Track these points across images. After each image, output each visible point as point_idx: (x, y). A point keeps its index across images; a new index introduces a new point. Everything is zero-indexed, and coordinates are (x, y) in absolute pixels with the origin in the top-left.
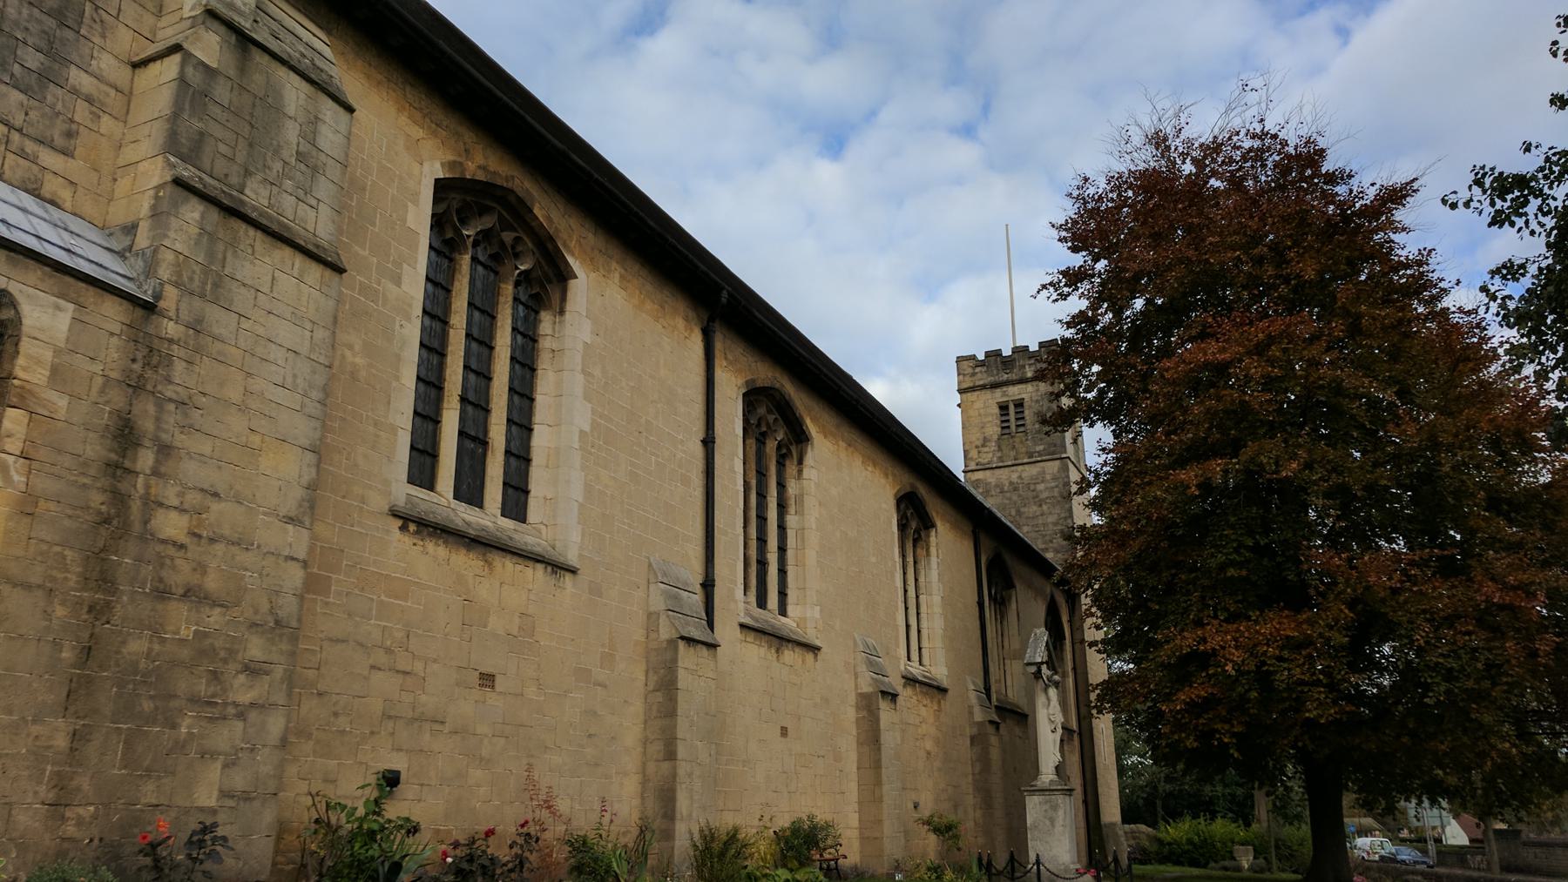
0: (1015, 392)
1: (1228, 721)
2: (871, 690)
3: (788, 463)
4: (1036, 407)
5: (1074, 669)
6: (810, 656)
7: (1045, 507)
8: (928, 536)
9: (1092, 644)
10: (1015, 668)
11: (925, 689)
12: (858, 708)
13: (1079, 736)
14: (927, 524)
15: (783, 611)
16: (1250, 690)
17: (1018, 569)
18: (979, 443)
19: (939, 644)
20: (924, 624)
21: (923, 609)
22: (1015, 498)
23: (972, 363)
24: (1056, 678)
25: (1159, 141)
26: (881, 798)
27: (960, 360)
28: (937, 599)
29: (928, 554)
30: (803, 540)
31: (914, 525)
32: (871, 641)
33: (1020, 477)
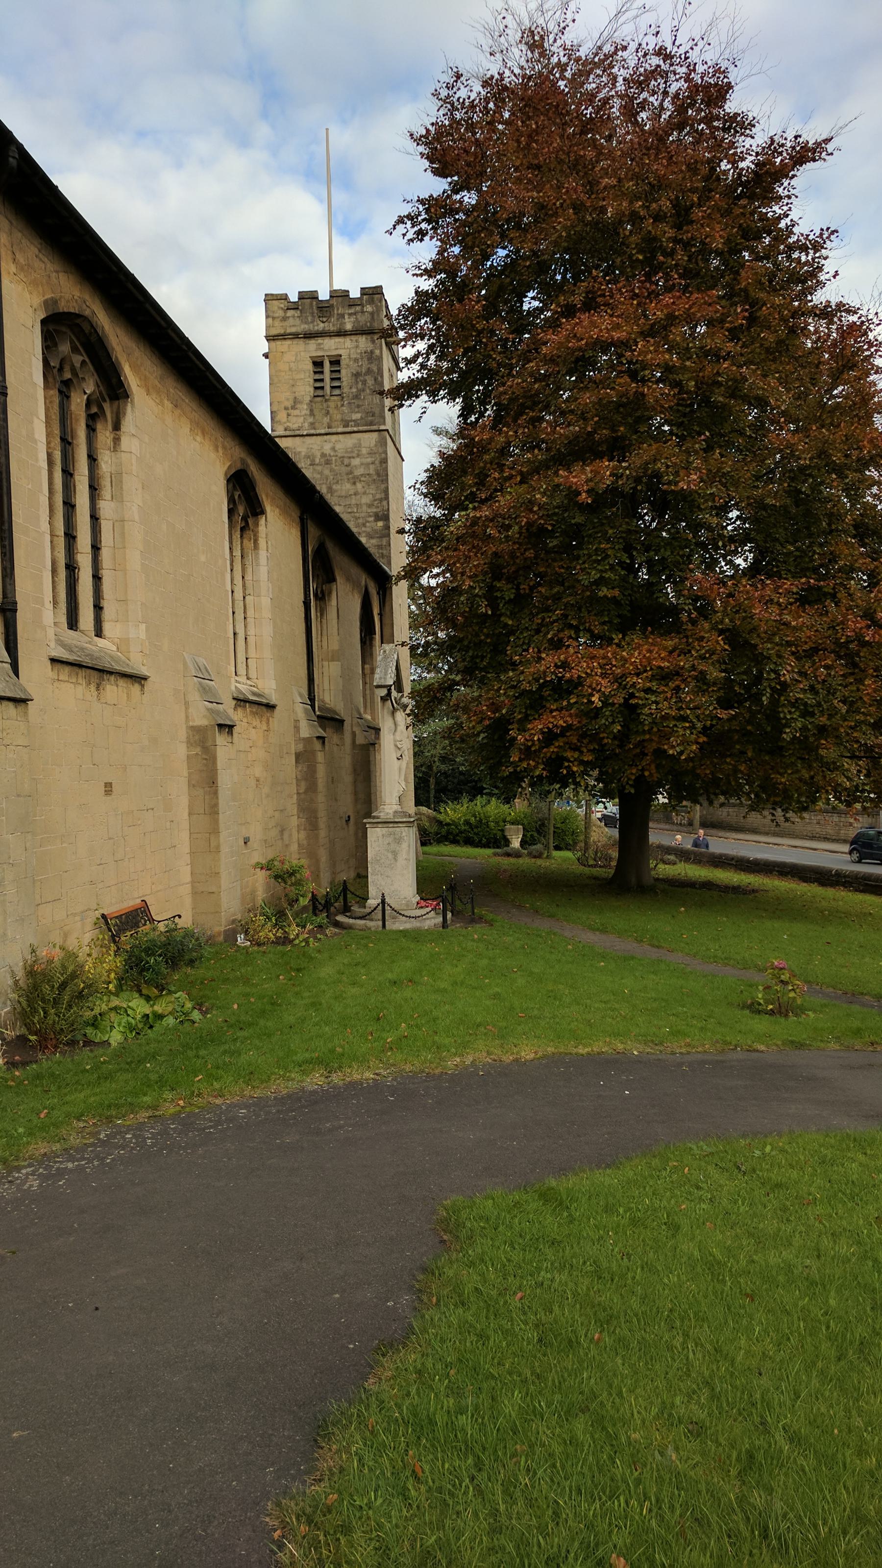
0: (331, 346)
1: (576, 749)
2: (204, 722)
3: (99, 426)
4: (354, 368)
6: (136, 688)
7: (359, 486)
8: (257, 525)
11: (255, 708)
12: (190, 743)
14: (256, 509)
15: (99, 633)
16: (613, 722)
17: (340, 560)
18: (289, 404)
19: (268, 654)
21: (250, 613)
22: (327, 472)
23: (283, 304)
25: (535, 42)
26: (218, 850)
27: (269, 299)
28: (266, 601)
29: (256, 547)
30: (123, 534)
32: (201, 661)
33: (333, 449)
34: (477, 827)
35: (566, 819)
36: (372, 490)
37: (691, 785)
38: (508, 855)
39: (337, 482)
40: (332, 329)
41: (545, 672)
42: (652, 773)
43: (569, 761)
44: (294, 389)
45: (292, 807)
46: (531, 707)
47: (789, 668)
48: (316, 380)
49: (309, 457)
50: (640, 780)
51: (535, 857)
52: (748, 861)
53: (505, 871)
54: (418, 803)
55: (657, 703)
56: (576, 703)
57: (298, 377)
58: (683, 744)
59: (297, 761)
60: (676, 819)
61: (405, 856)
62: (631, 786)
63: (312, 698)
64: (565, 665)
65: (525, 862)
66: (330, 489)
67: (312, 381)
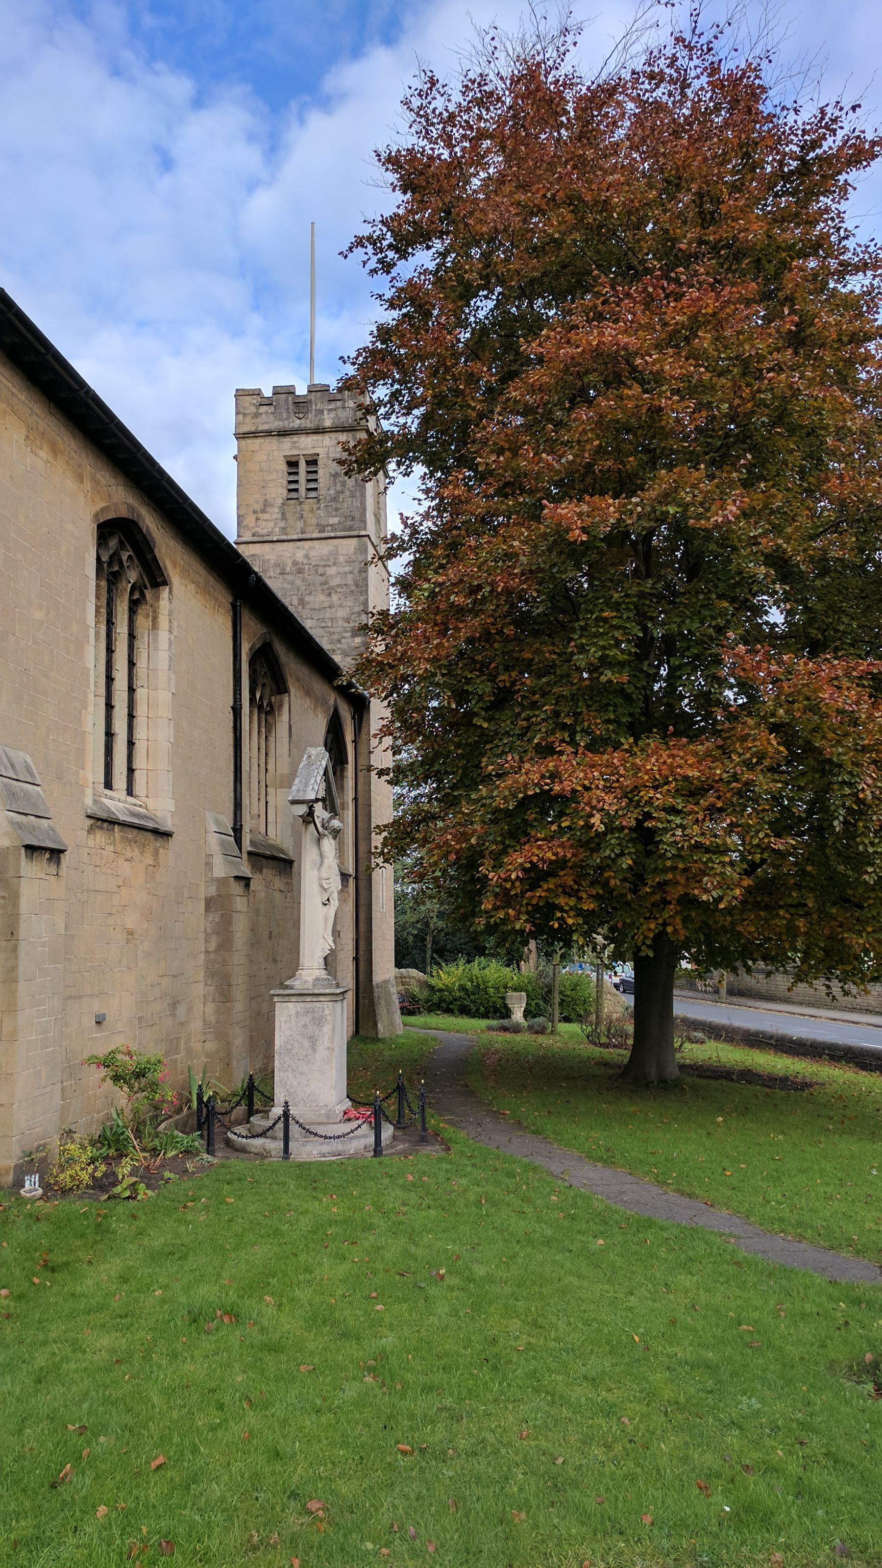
0: (307, 445)
5: (356, 799)
7: (335, 597)
8: (157, 598)
9: (381, 773)
10: (279, 798)
11: (131, 834)
13: (358, 883)
15: (130, 792)
16: (622, 854)
17: (293, 667)
18: (258, 507)
19: (162, 764)
20: (140, 734)
21: (141, 710)
22: (298, 582)
23: (255, 400)
24: (336, 823)
27: (240, 394)
28: (164, 696)
31: (133, 576)
33: (307, 556)
34: (474, 993)
35: (576, 985)
36: (349, 602)
37: (727, 948)
38: (505, 1029)
39: (310, 594)
40: (309, 425)
41: (526, 785)
42: (677, 930)
43: (562, 910)
44: (264, 491)
45: (196, 970)
46: (512, 835)
47: (870, 781)
48: (290, 482)
49: (279, 565)
50: (660, 938)
51: (537, 1032)
52: (791, 1041)
53: (497, 1051)
54: (399, 964)
55: (683, 827)
56: (569, 827)
57: (270, 478)
58: (722, 886)
59: (207, 909)
60: (699, 984)
61: (326, 1044)
62: (648, 946)
63: (237, 831)
64: (554, 776)
65: (523, 1039)
66: (302, 602)
67: (285, 482)
